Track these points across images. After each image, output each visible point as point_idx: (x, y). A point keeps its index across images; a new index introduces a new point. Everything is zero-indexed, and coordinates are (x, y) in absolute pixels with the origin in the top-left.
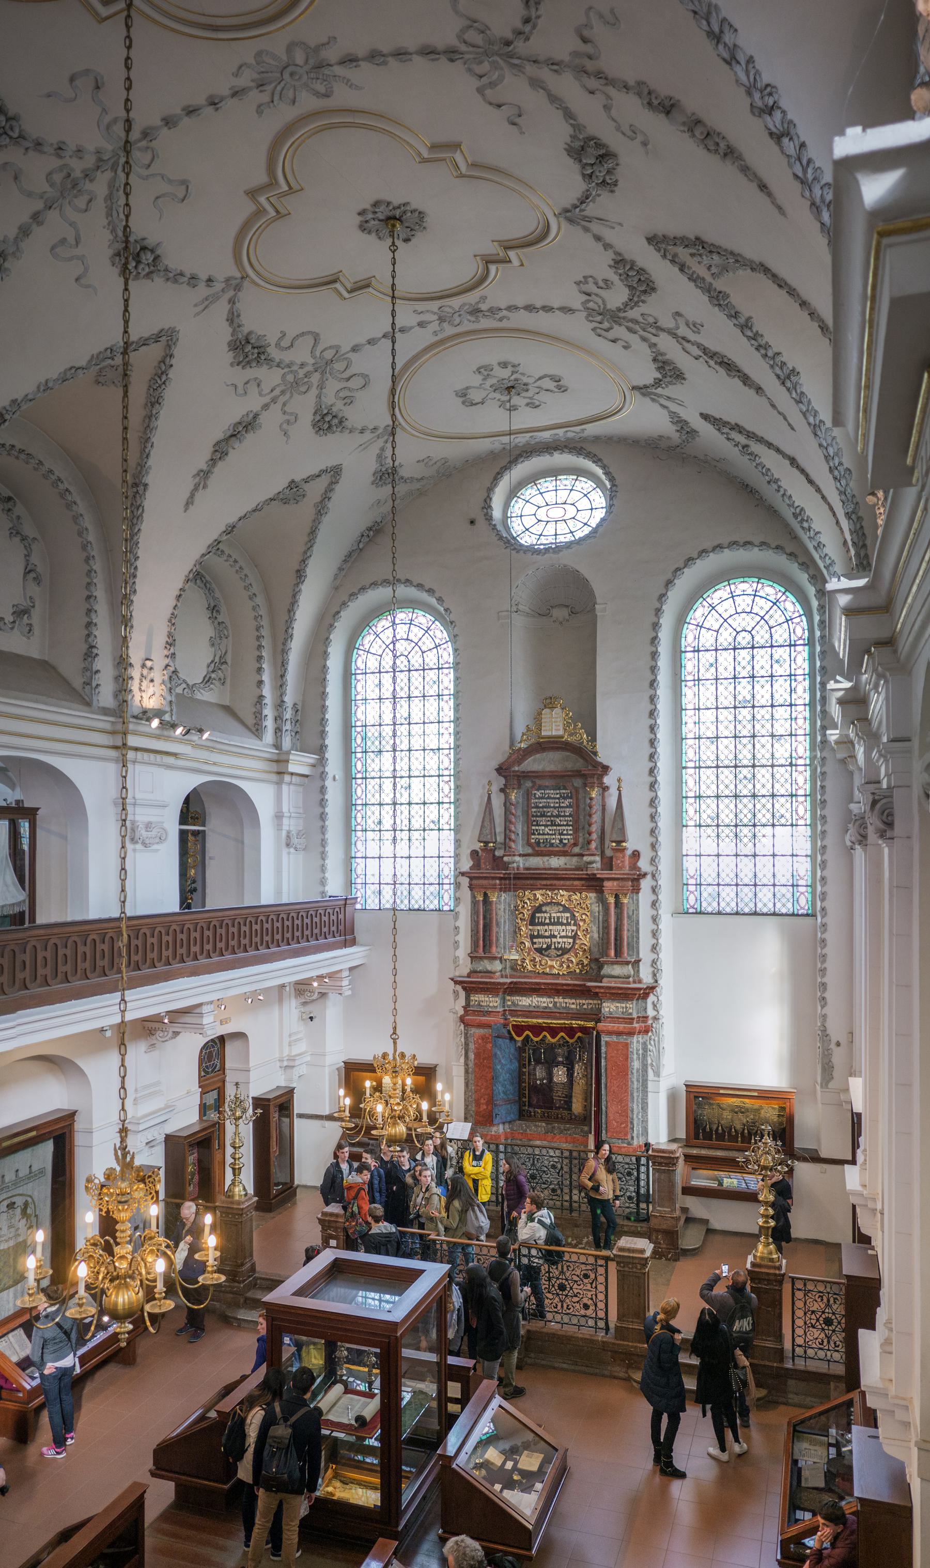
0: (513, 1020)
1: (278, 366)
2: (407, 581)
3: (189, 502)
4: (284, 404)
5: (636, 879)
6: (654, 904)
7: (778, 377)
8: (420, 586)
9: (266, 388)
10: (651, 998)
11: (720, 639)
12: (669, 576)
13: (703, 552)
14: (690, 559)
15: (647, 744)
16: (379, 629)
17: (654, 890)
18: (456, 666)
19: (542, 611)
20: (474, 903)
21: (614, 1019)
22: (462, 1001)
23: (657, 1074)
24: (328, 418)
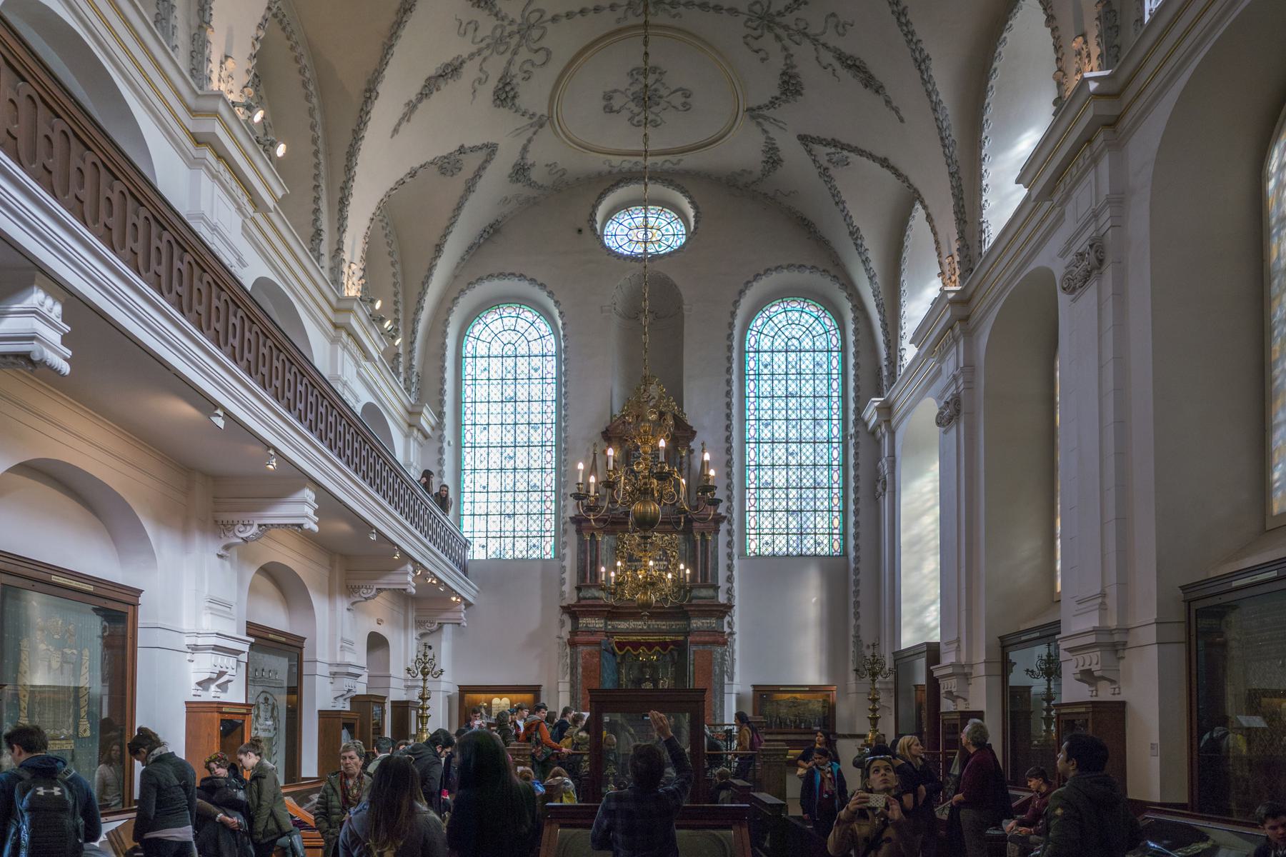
0: (616, 639)
1: (496, 15)
2: (521, 275)
3: (396, 131)
4: (485, 60)
5: (719, 519)
6: (730, 544)
7: (916, 60)
8: (533, 281)
9: (480, 35)
10: (727, 619)
11: (776, 344)
12: (742, 287)
13: (767, 271)
14: (758, 275)
15: (723, 416)
16: (489, 320)
17: (730, 533)
18: (558, 355)
19: (632, 314)
20: (581, 543)
21: (700, 631)
22: (568, 627)
23: (731, 679)
24: (508, 89)
